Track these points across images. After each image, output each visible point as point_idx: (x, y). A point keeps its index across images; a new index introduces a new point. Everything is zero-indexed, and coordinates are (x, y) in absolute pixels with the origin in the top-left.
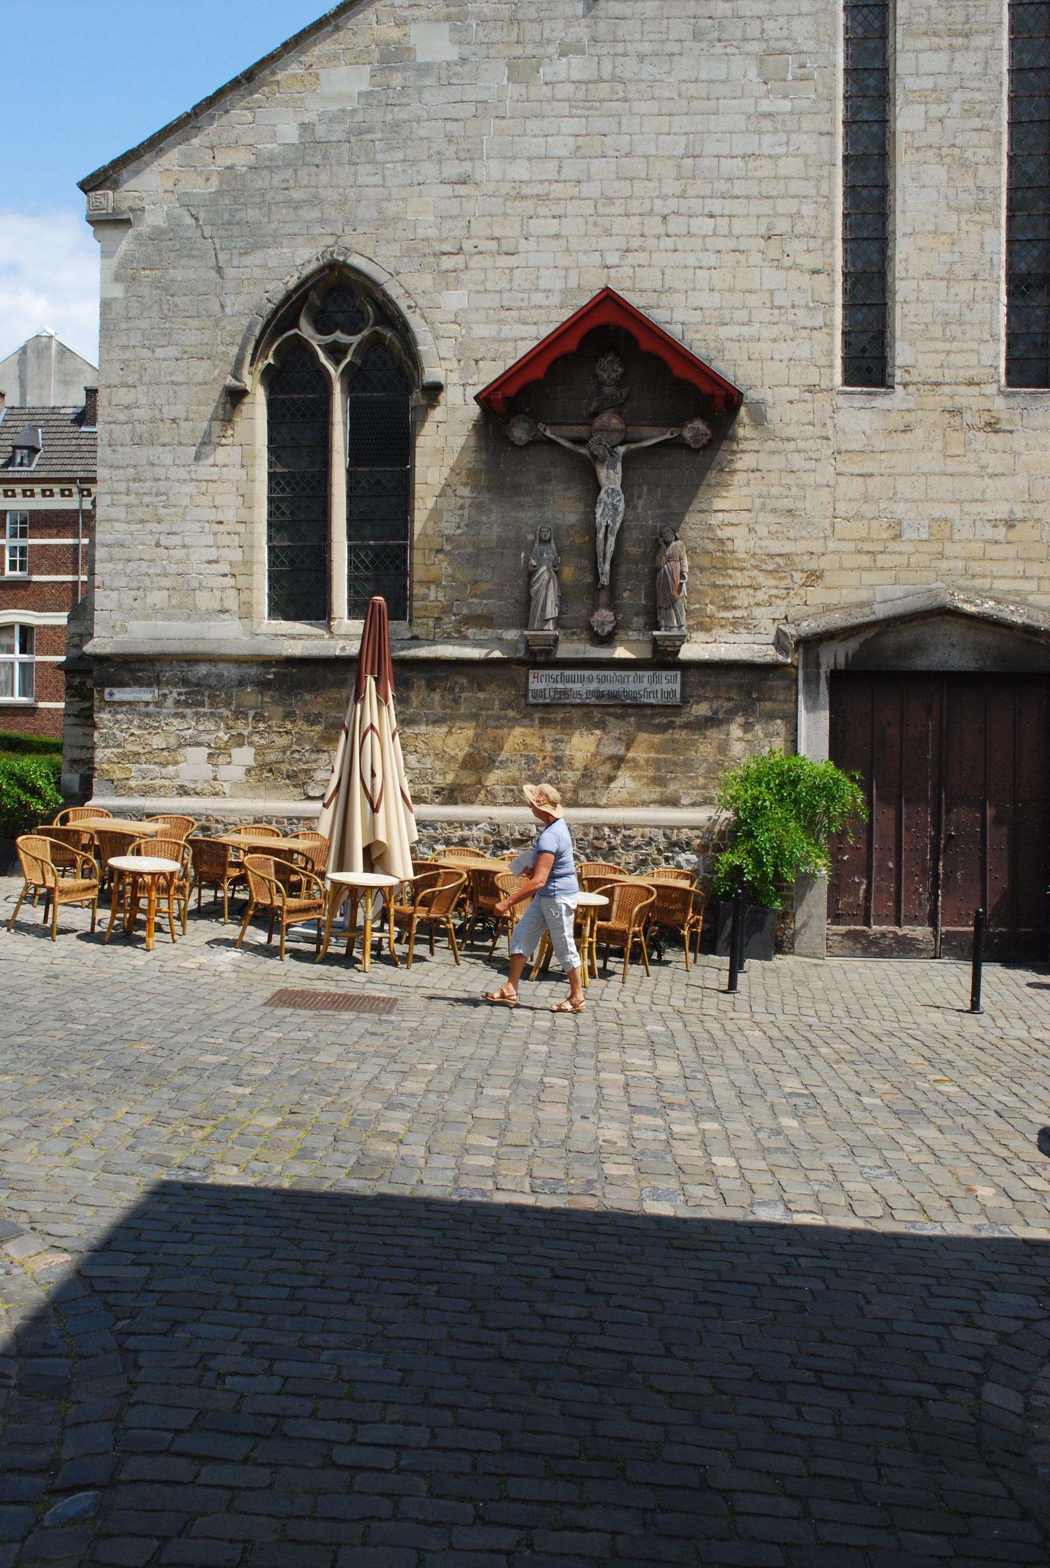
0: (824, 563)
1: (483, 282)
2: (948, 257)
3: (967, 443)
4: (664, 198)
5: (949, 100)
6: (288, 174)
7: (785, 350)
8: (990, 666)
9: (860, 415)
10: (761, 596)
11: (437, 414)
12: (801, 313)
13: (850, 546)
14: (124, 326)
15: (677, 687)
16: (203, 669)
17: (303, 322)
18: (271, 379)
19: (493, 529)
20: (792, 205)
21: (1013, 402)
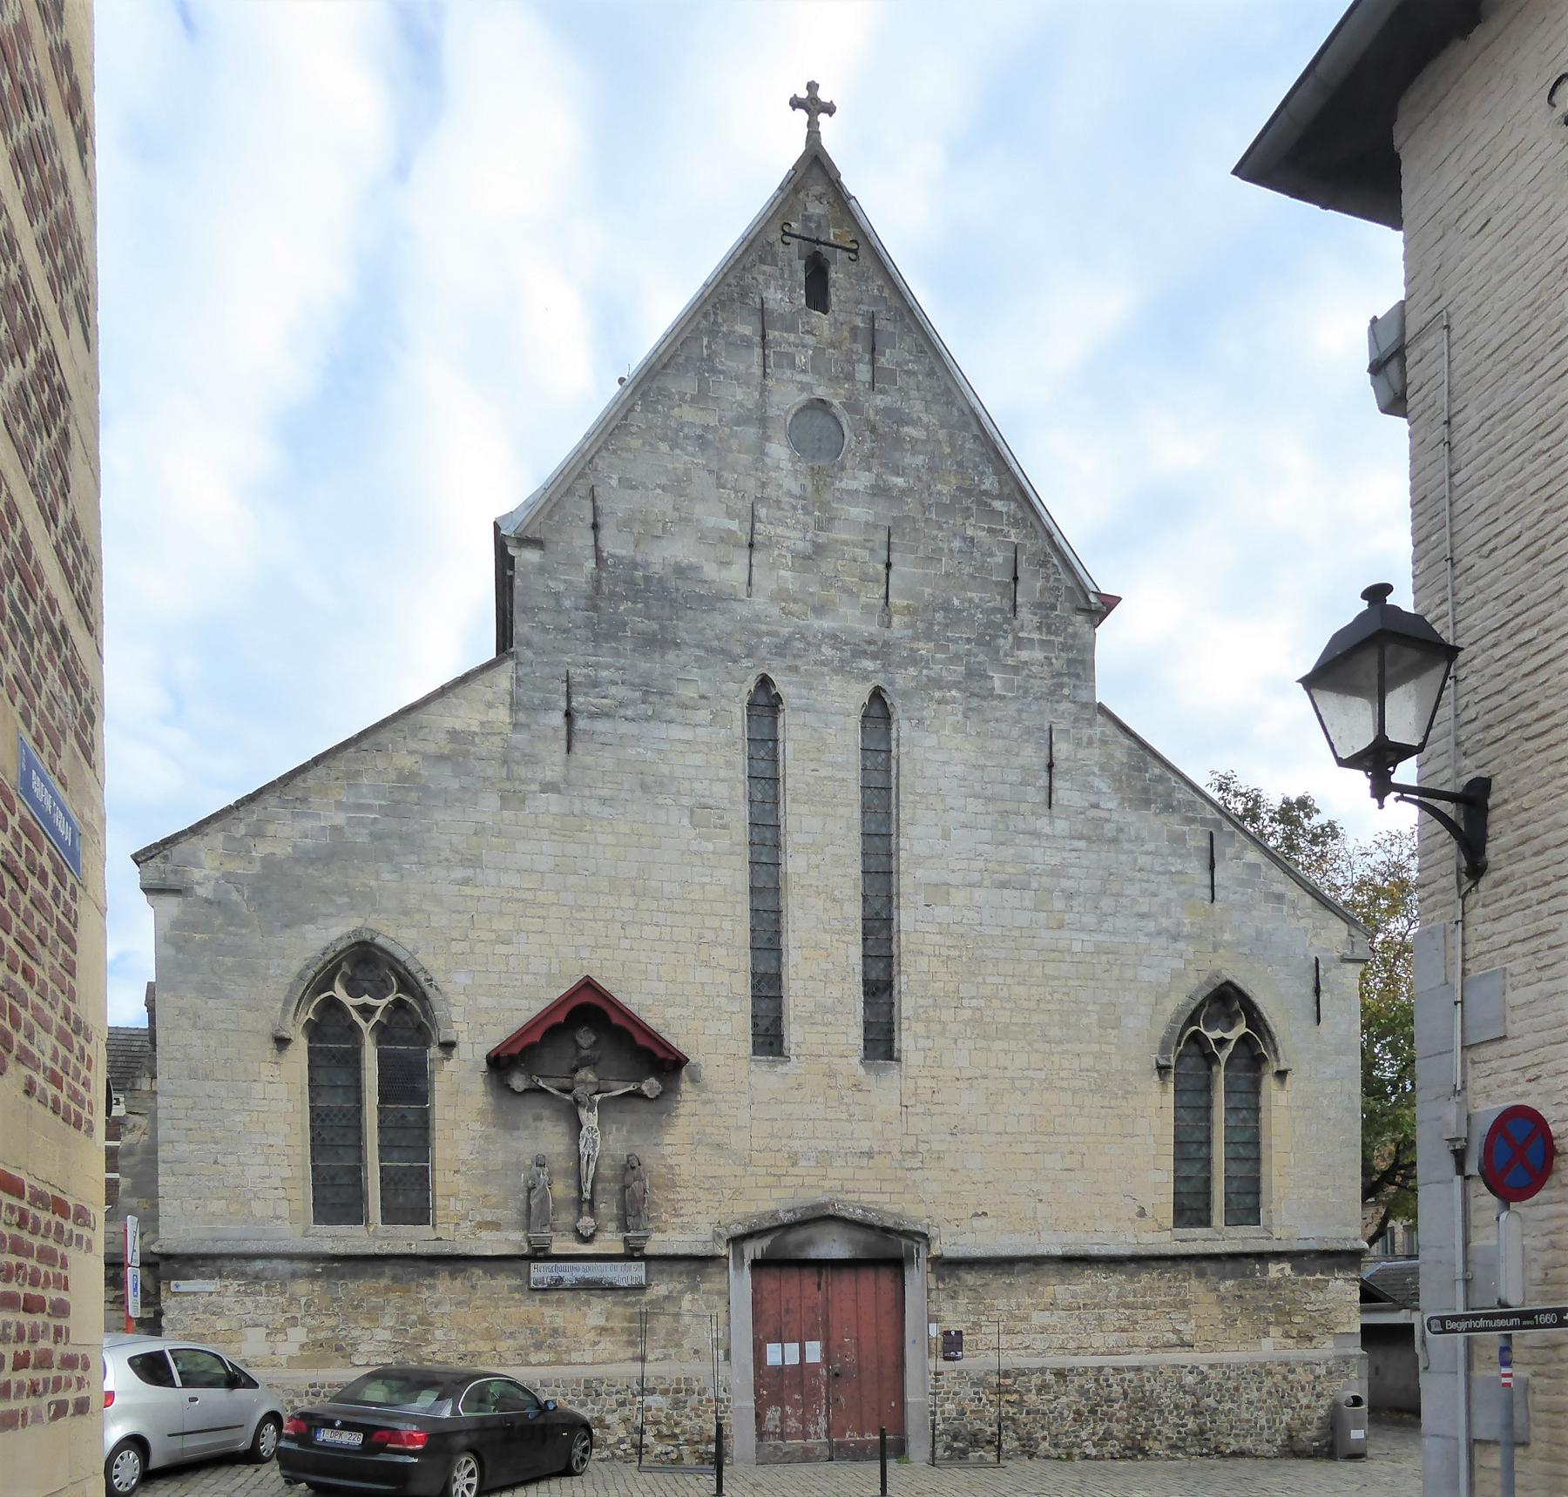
2: (824, 966)
8: (860, 1255)
9: (767, 1078)
10: (701, 1207)
12: (723, 1000)
13: (762, 1171)
16: (259, 1265)
17: (337, 985)
18: (314, 1031)
20: (715, 922)
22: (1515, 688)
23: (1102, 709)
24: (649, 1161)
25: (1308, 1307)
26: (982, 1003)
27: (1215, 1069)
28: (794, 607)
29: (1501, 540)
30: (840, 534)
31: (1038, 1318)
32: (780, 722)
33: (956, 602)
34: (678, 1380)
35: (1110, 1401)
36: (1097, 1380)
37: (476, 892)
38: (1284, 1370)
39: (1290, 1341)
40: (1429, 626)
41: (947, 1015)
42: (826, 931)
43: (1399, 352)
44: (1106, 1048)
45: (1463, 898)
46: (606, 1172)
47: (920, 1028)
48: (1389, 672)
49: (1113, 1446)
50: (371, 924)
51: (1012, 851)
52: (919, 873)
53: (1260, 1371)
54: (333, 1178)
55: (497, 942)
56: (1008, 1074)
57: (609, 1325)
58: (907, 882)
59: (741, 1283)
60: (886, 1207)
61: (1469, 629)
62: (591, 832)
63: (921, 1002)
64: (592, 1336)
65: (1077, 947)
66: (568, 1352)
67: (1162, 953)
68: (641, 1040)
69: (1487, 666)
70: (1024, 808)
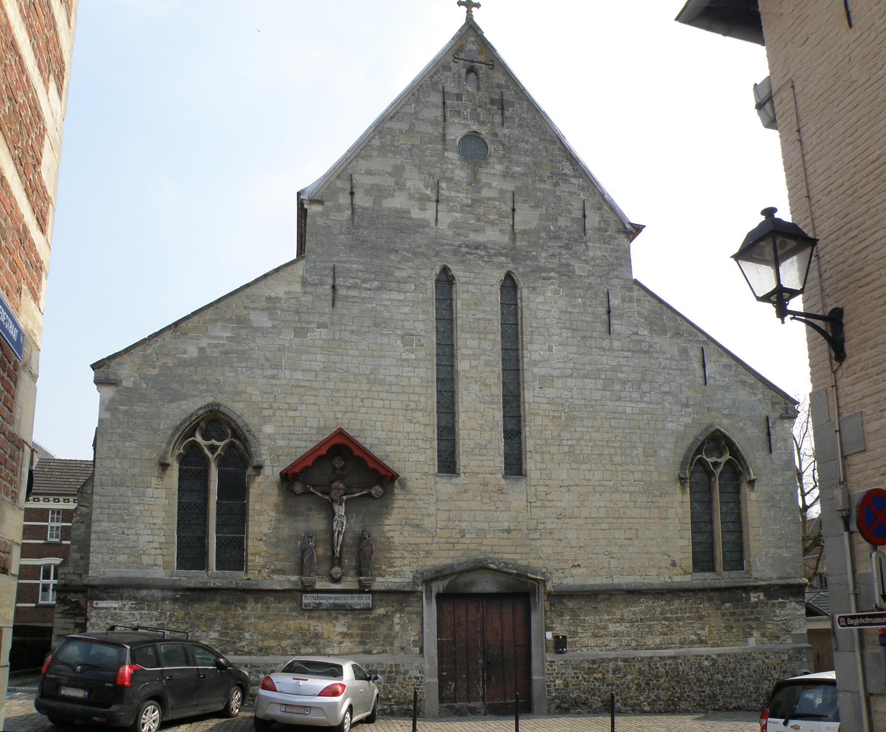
0: (433, 547)
1: (282, 422)
3: (490, 498)
4: (362, 391)
5: (479, 359)
6: (192, 369)
7: (414, 457)
8: (503, 590)
9: (446, 486)
10: (406, 561)
11: (259, 479)
12: (420, 442)
13: (443, 540)
14: (110, 431)
15: (370, 601)
16: (144, 592)
18: (183, 460)
19: (285, 532)
21: (509, 481)
22: (850, 261)
23: (636, 282)
24: (375, 535)
25: (775, 619)
26: (575, 442)
27: (713, 479)
28: (460, 231)
29: (833, 186)
30: (486, 193)
31: (612, 628)
32: (454, 290)
33: (552, 228)
34: (391, 666)
35: (657, 677)
36: (649, 666)
37: (278, 382)
38: (762, 656)
39: (765, 639)
40: (800, 230)
41: (554, 450)
42: (481, 402)
43: (770, 99)
44: (648, 468)
45: (835, 372)
46: (349, 541)
47: (538, 457)
48: (780, 252)
49: (660, 705)
50: (219, 401)
51: (589, 358)
52: (535, 370)
53: (747, 658)
54: (189, 543)
55: (289, 409)
56: (591, 483)
57: (349, 632)
58: (528, 374)
59: (430, 611)
60: (519, 562)
61: (823, 230)
62: (345, 349)
63: (538, 442)
64: (338, 638)
65: (629, 410)
66: (325, 646)
67: (678, 414)
68: (371, 464)
69: (834, 249)
70: (595, 334)
